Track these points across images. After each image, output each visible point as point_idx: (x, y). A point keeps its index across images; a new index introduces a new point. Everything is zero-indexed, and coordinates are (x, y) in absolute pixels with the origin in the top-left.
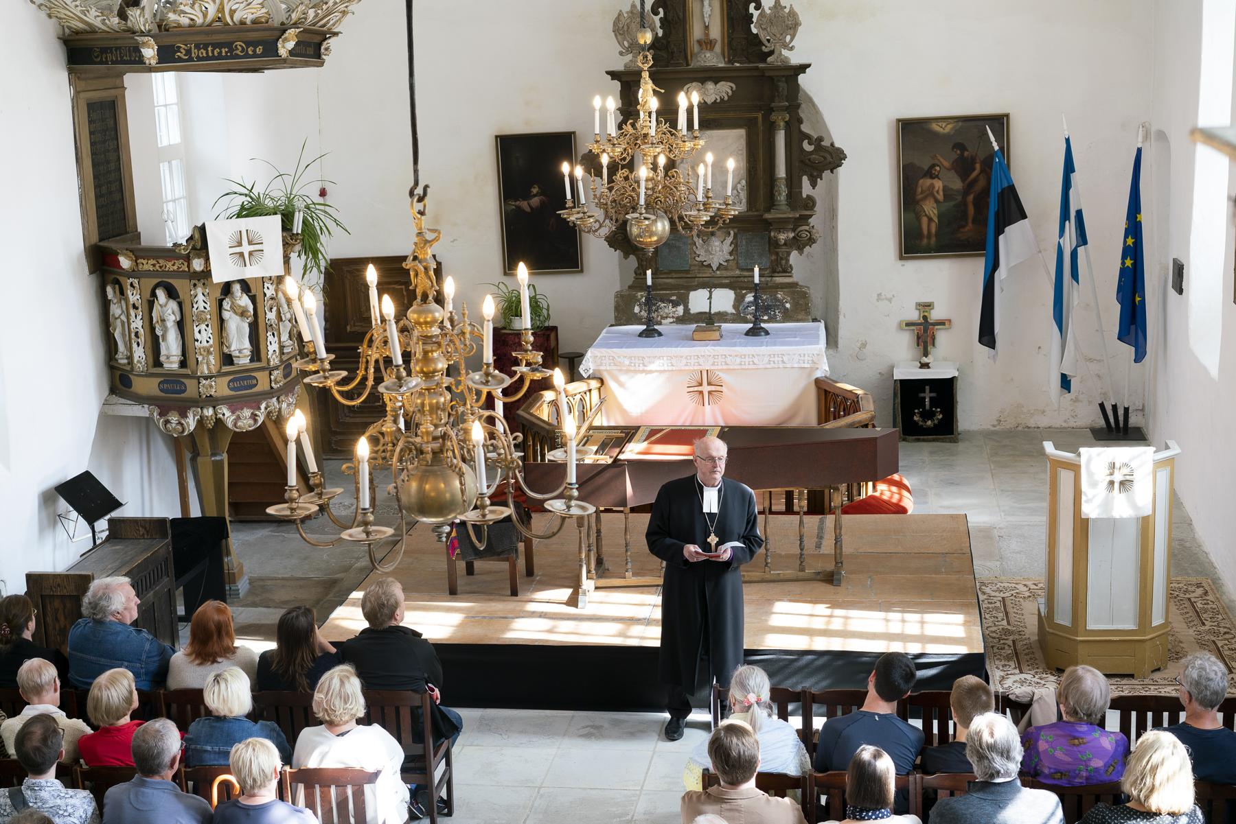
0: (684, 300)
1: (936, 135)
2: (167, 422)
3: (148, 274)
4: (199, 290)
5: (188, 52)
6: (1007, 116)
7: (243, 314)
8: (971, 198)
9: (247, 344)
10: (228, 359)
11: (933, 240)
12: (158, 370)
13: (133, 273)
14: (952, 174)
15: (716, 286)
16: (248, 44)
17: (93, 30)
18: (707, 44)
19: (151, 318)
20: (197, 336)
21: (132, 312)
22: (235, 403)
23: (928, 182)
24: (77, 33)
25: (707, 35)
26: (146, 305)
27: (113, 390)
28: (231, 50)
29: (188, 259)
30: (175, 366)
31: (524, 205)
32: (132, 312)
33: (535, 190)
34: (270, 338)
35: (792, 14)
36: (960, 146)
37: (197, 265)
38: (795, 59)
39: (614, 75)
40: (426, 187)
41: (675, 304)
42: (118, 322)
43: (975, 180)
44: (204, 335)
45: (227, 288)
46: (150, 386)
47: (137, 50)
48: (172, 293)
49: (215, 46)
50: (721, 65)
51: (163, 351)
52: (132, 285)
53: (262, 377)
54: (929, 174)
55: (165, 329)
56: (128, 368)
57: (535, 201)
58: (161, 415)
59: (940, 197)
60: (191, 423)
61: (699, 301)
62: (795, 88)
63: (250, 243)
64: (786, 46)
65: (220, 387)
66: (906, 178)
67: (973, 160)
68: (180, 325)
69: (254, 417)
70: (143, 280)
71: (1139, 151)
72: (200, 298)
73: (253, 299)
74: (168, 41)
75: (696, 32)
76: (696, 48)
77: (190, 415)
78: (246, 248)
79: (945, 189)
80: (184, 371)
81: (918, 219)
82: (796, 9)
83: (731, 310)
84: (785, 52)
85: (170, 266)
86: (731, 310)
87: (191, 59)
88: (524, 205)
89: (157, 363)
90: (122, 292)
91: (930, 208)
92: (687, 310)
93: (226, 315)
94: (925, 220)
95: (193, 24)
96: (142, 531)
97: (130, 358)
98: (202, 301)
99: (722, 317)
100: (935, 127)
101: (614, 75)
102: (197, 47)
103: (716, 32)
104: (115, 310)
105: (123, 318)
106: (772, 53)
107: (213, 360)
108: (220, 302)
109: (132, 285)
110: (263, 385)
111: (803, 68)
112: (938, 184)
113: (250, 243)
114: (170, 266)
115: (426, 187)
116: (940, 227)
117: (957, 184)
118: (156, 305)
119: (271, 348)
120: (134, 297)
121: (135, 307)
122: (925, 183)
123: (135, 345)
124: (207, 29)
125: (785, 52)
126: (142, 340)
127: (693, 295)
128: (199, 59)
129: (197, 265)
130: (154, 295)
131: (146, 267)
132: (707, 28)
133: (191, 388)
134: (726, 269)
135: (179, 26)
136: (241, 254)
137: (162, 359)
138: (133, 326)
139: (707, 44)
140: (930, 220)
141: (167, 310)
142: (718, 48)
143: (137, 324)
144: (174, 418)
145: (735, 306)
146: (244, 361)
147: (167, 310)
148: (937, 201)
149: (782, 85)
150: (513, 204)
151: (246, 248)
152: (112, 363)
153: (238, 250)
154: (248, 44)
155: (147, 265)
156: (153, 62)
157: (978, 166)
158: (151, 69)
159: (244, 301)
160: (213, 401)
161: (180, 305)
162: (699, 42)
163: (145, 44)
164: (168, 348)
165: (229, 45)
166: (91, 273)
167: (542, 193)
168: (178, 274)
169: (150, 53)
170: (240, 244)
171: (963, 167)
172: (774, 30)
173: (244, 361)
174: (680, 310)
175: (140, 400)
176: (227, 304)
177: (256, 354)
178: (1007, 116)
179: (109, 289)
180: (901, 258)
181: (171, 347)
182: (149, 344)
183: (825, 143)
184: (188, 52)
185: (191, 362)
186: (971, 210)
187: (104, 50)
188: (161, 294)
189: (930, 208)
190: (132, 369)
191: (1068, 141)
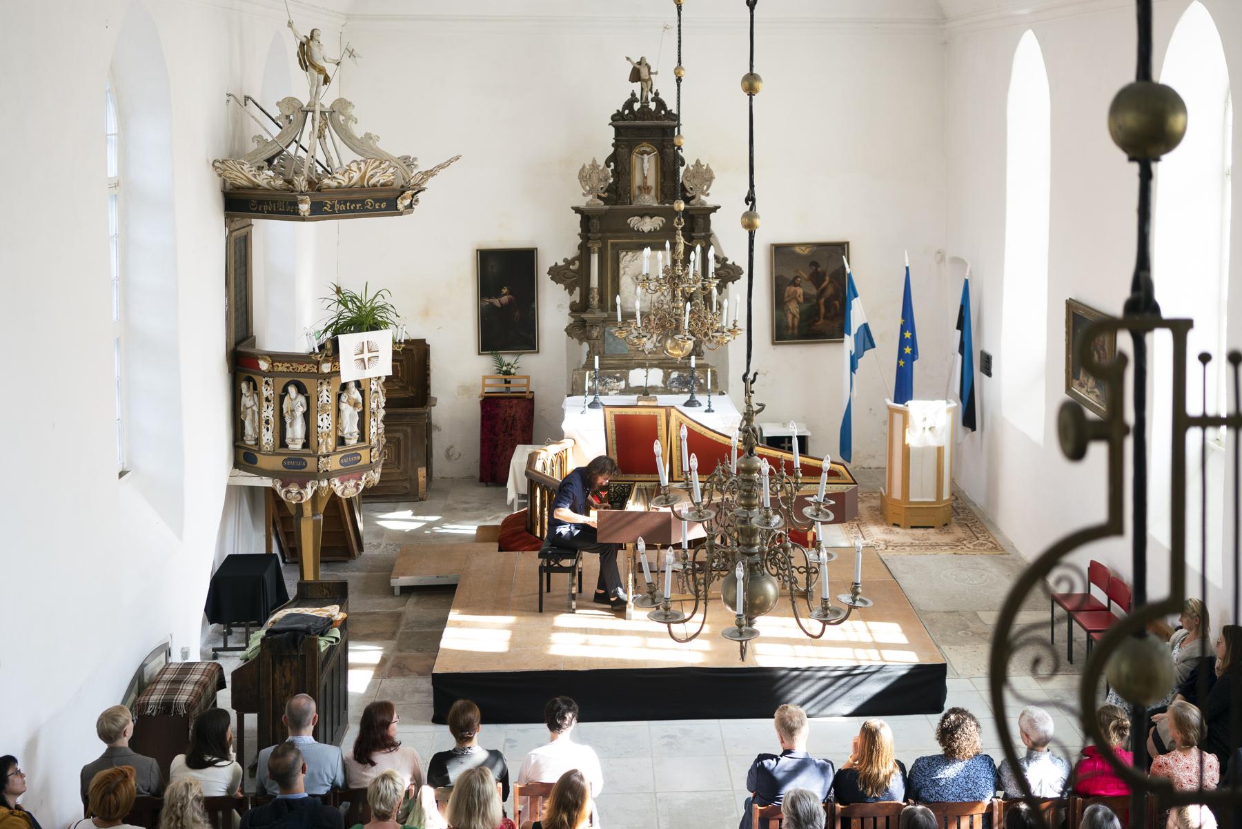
0: (625, 377)
1: (799, 255)
2: (288, 492)
3: (282, 374)
4: (325, 387)
5: (332, 206)
6: (848, 243)
7: (355, 405)
8: (822, 301)
9: (356, 429)
10: (341, 441)
11: (796, 331)
12: (283, 450)
13: (270, 373)
14: (810, 283)
15: (652, 366)
16: (376, 201)
17: (256, 187)
18: (645, 189)
19: (281, 410)
20: (320, 423)
21: (265, 404)
22: (343, 475)
23: (793, 288)
24: (239, 188)
25: (645, 183)
26: (277, 399)
27: (237, 465)
28: (363, 205)
29: (318, 363)
30: (299, 447)
31: (496, 302)
32: (265, 404)
33: (505, 291)
34: (373, 423)
35: (708, 170)
36: (815, 264)
37: (326, 368)
38: (710, 201)
39: (577, 210)
40: (756, 374)
41: (619, 380)
42: (249, 411)
43: (825, 289)
44: (325, 422)
45: (344, 387)
46: (277, 463)
47: (295, 204)
48: (301, 390)
49: (352, 202)
50: (656, 205)
51: (289, 434)
52: (267, 383)
53: (364, 454)
54: (794, 283)
55: (293, 418)
56: (256, 448)
57: (505, 299)
58: (283, 486)
59: (801, 300)
60: (309, 493)
61: (637, 377)
62: (708, 222)
63: (369, 351)
64: (703, 193)
65: (334, 463)
66: (777, 286)
67: (824, 274)
68: (306, 416)
69: (357, 485)
70: (277, 379)
71: (967, 281)
72: (325, 393)
73: (362, 393)
74: (319, 198)
75: (637, 180)
76: (637, 192)
77: (309, 486)
78: (366, 355)
79: (804, 294)
80: (306, 451)
81: (786, 315)
82: (711, 167)
83: (660, 384)
84: (703, 198)
85: (301, 368)
86: (660, 384)
87: (334, 212)
88: (496, 302)
89: (283, 444)
90: (255, 388)
91: (794, 308)
92: (627, 384)
93: (344, 406)
94: (790, 317)
95: (339, 187)
96: (326, 592)
97: (258, 440)
98: (326, 394)
99: (654, 389)
100: (798, 250)
101: (577, 210)
102: (339, 203)
103: (651, 182)
104: (247, 401)
105: (255, 408)
106: (693, 197)
107: (331, 442)
108: (339, 396)
109: (267, 383)
110: (365, 460)
111: (715, 209)
112: (800, 291)
113: (369, 351)
114: (301, 368)
115: (756, 374)
116: (800, 321)
117: (813, 291)
118: (287, 398)
119: (373, 430)
120: (266, 392)
121: (267, 400)
122: (791, 289)
123: (264, 430)
124: (350, 189)
125: (703, 198)
126: (271, 427)
127: (632, 373)
128: (340, 212)
129: (326, 368)
130: (285, 391)
131: (280, 369)
132: (645, 178)
133: (311, 463)
134: (655, 353)
135: (329, 187)
136: (363, 360)
137: (288, 441)
138: (264, 415)
139: (645, 189)
140: (794, 316)
141: (295, 402)
142: (653, 192)
143: (269, 413)
144: (294, 489)
145: (664, 382)
146: (352, 442)
147: (295, 402)
148: (799, 303)
149: (701, 221)
150: (487, 301)
151: (366, 355)
152: (239, 443)
153: (360, 356)
154: (376, 201)
155: (281, 367)
156: (307, 214)
157: (827, 278)
158: (304, 219)
159: (356, 395)
160: (329, 475)
161: (307, 399)
162: (639, 188)
163: (302, 201)
164: (293, 432)
165: (363, 202)
166: (1118, 574)
167: (511, 293)
168: (308, 375)
169: (304, 208)
170: (362, 352)
171: (817, 278)
172: (696, 181)
173: (352, 442)
174: (622, 384)
175: (262, 473)
176: (344, 398)
177: (362, 438)
178: (848, 243)
179: (244, 386)
180: (773, 343)
181: (296, 431)
182: (278, 430)
183: (729, 262)
184: (332, 206)
185: (313, 443)
186: (823, 310)
187: (260, 202)
188: (292, 390)
189: (794, 308)
190: (260, 449)
191: (967, 281)
